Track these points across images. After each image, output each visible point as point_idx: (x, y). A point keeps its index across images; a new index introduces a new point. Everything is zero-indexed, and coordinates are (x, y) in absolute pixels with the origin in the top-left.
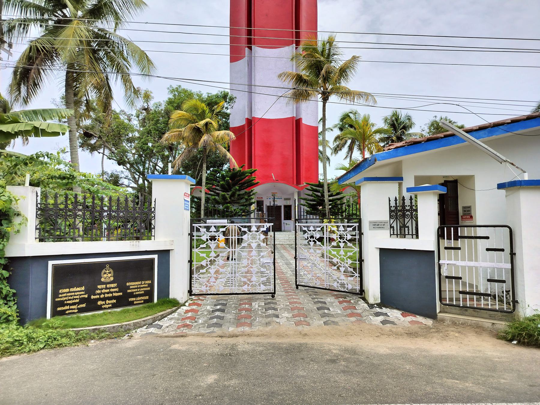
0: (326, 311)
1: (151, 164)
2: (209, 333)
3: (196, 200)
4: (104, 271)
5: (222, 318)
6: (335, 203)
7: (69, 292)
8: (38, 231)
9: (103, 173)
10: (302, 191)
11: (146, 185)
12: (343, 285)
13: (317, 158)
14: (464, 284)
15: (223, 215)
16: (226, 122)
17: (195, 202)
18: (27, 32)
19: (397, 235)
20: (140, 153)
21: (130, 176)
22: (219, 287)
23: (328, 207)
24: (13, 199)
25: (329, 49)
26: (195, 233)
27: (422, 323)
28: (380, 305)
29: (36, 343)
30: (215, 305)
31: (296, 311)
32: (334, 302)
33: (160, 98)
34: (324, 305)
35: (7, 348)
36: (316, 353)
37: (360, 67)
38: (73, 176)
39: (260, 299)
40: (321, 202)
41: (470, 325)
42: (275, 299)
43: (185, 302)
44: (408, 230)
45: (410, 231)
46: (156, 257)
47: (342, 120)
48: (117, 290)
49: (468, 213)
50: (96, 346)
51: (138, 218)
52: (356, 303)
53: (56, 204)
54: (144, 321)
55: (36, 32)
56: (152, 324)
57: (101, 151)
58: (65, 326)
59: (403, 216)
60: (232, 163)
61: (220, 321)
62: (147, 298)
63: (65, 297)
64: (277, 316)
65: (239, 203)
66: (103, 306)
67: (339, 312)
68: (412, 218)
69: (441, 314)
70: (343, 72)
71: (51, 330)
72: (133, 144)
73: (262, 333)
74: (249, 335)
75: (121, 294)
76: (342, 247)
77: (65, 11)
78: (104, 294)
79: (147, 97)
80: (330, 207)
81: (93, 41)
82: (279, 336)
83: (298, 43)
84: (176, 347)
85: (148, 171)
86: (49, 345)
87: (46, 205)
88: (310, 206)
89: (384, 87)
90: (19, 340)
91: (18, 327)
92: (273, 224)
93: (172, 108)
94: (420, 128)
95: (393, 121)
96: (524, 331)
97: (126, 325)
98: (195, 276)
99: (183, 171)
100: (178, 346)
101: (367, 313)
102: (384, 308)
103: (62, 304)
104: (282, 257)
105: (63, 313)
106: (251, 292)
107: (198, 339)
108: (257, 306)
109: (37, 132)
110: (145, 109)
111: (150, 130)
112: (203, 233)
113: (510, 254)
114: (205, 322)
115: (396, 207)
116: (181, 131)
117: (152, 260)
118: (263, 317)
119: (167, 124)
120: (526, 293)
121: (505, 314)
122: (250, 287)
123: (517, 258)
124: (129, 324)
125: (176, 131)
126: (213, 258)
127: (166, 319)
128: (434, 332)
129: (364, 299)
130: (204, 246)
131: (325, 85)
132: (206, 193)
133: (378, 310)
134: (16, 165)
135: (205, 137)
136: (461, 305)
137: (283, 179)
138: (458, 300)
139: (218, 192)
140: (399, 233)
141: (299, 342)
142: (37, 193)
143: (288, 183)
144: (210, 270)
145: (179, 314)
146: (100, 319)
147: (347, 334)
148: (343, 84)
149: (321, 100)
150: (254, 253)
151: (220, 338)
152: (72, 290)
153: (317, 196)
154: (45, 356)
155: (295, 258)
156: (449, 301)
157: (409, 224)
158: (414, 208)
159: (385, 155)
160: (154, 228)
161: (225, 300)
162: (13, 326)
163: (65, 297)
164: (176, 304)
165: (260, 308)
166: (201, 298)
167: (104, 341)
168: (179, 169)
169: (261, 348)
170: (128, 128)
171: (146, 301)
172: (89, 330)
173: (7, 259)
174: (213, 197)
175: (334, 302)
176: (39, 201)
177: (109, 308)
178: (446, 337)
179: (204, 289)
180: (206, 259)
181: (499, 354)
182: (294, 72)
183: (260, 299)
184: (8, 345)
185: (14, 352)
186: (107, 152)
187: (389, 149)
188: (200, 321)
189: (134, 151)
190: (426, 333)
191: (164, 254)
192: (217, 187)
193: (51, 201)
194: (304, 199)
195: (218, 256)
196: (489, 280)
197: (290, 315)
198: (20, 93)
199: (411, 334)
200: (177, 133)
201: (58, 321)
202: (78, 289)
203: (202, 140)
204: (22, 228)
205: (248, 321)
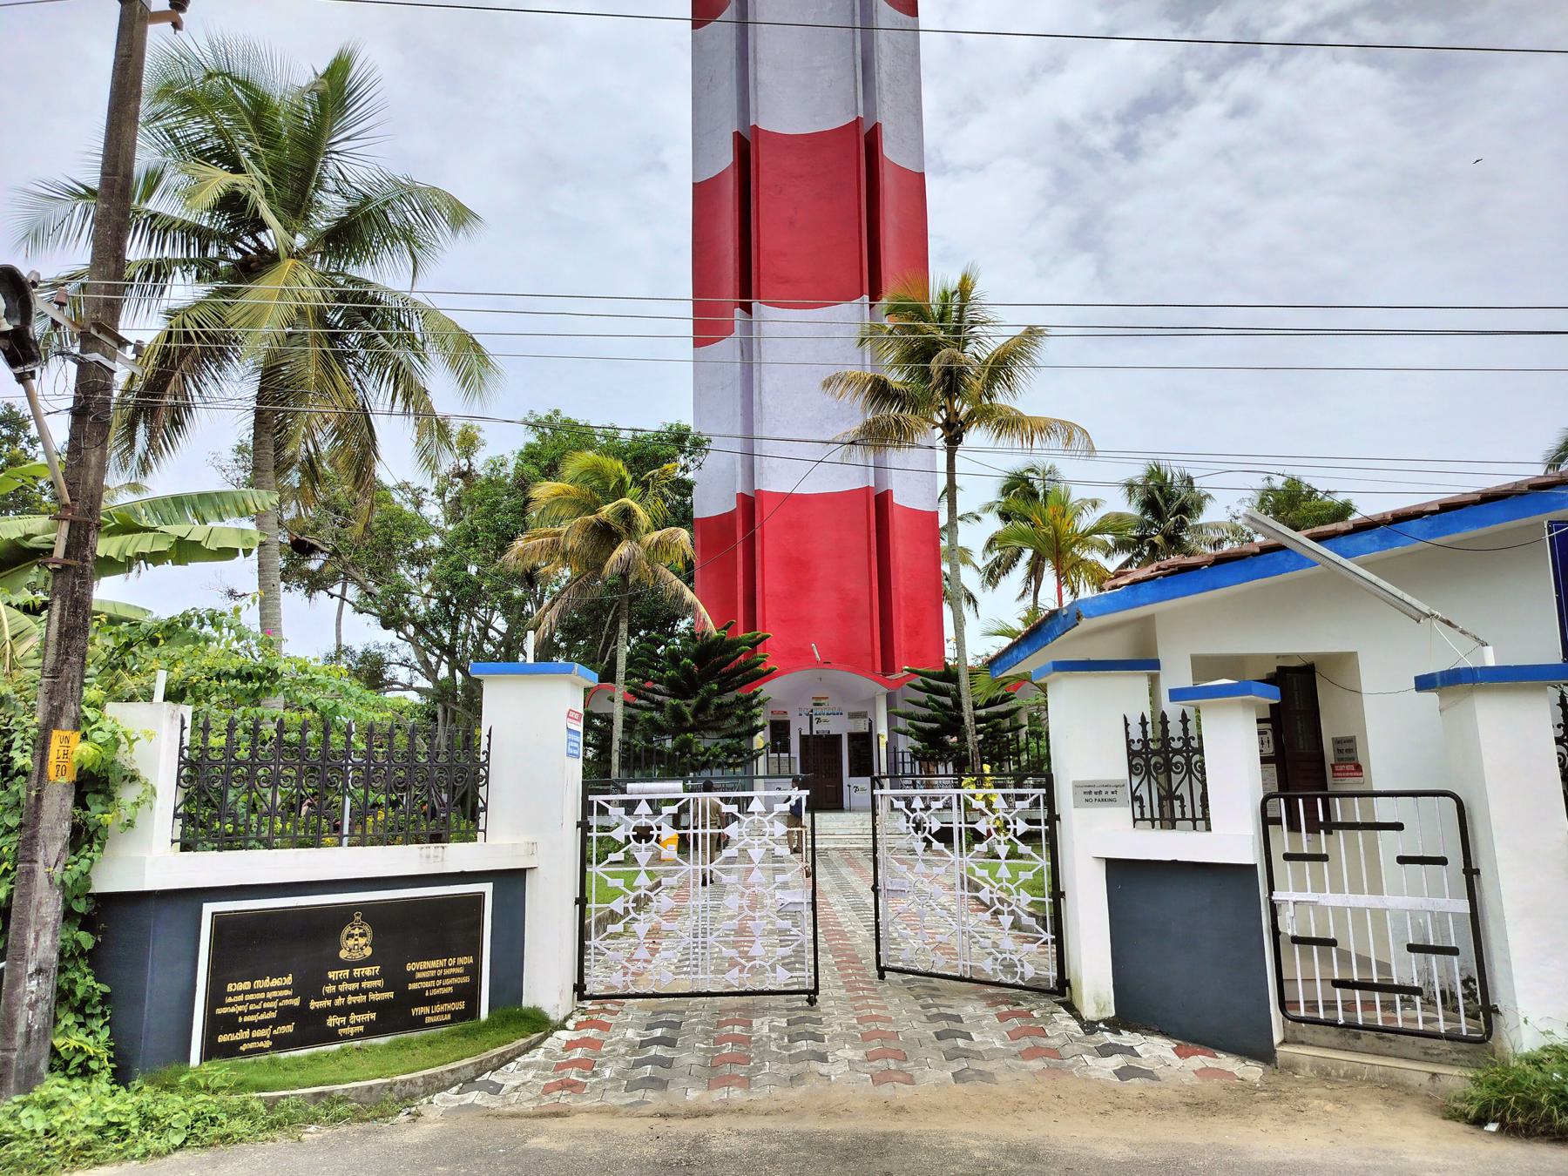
0: (961, 1042)
1: (474, 622)
2: (631, 1104)
3: (597, 722)
4: (348, 929)
5: (666, 1063)
6: (993, 727)
7: (252, 991)
8: (180, 821)
9: (341, 651)
10: (899, 693)
11: (459, 683)
12: (1009, 967)
13: (939, 596)
14: (1345, 957)
15: (673, 767)
16: (682, 503)
17: (596, 729)
18: (162, 292)
19: (1153, 820)
20: (443, 594)
21: (414, 659)
22: (662, 973)
23: (973, 739)
24: (123, 739)
25: (961, 310)
26: (594, 820)
27: (1232, 1073)
28: (1114, 1025)
29: (163, 1130)
30: (650, 1027)
31: (875, 1042)
32: (984, 1017)
33: (502, 446)
34: (956, 1026)
35: (87, 1146)
36: (926, 1158)
37: (1048, 351)
38: (274, 672)
39: (776, 1008)
40: (954, 724)
41: (1369, 1081)
42: (818, 1009)
43: (566, 1020)
44: (1183, 806)
45: (1188, 810)
46: (487, 888)
47: (1006, 491)
48: (379, 983)
49: (1350, 755)
50: (322, 1141)
51: (445, 789)
52: (1047, 1018)
53: (230, 749)
54: (452, 1071)
55: (183, 290)
56: (473, 1080)
57: (337, 589)
58: (240, 1087)
59: (1164, 767)
60: (700, 617)
61: (662, 1073)
62: (461, 1005)
63: (240, 1003)
64: (822, 1058)
65: (718, 729)
66: (341, 1031)
67: (998, 1044)
68: (1190, 772)
69: (1286, 1049)
70: (1000, 368)
71: (201, 1097)
72: (425, 570)
73: (780, 1104)
74: (742, 1112)
75: (390, 995)
76: (1003, 856)
77: (262, 236)
78: (345, 994)
79: (469, 443)
80: (981, 737)
81: (330, 308)
82: (825, 1112)
83: (875, 295)
84: (540, 1142)
85: (464, 644)
86: (197, 1138)
87: (205, 751)
88: (922, 735)
89: (1101, 419)
90: (119, 1124)
91: (115, 1087)
92: (807, 792)
93: (535, 471)
94: (1227, 508)
95: (1150, 492)
96: (1512, 1092)
97: (404, 1083)
98: (593, 942)
99: (561, 640)
100: (547, 1139)
101: (1076, 1048)
102: (1125, 1033)
103: (232, 1024)
104: (843, 886)
105: (231, 1050)
106: (749, 987)
107: (602, 1123)
108: (766, 1029)
109: (185, 551)
110: (462, 475)
111: (475, 530)
112: (616, 820)
113: (1465, 871)
114: (621, 1074)
115: (1145, 742)
116: (558, 534)
117: (479, 898)
118: (781, 1060)
119: (524, 513)
120: (1518, 983)
121: (1465, 1046)
122: (745, 975)
123: (1485, 881)
124: (411, 1081)
125: (546, 535)
126: (642, 892)
127: (512, 1065)
128: (1264, 1099)
129: (1070, 1007)
130: (620, 856)
131: (951, 403)
132: (626, 704)
133: (1109, 1038)
134: (129, 645)
135: (623, 550)
136: (1341, 1021)
137: (844, 658)
138: (1330, 1005)
139: (658, 698)
140: (1157, 815)
141: (881, 1129)
142: (183, 721)
143: (858, 669)
144: (635, 926)
145: (548, 1053)
146: (333, 1067)
147: (1017, 1107)
148: (1002, 398)
149: (941, 443)
150: (757, 876)
151: (662, 1120)
152: (258, 984)
153: (942, 706)
154: (188, 1166)
155: (875, 889)
156: (1325, 1008)
157: (1183, 790)
158: (1195, 744)
159: (1104, 601)
160: (485, 809)
161: (677, 1012)
162: (102, 1084)
163: (240, 1003)
164: (539, 1024)
165: (773, 1035)
166: (609, 1006)
167: (344, 1129)
168: (552, 635)
169: (775, 1147)
170: (413, 526)
171: (457, 1017)
172: (303, 1095)
173: (91, 900)
174: (647, 715)
175: (984, 1017)
176: (186, 743)
177: (357, 1036)
178: (1296, 1114)
179: (618, 982)
180: (626, 895)
181: (1440, 1161)
182: (869, 372)
183: (776, 1008)
184: (90, 1137)
185: (105, 1157)
186: (352, 592)
187: (1115, 587)
188: (607, 1073)
189: (426, 589)
190: (1243, 1100)
191: (511, 882)
192: (658, 686)
193: (216, 741)
194: (906, 716)
195: (659, 884)
196: (1412, 948)
197: (858, 1055)
198: (132, 445)
199: (1199, 1106)
200: (549, 537)
201: (220, 1071)
202: (276, 982)
203: (615, 556)
204: (140, 816)
205: (740, 1071)
